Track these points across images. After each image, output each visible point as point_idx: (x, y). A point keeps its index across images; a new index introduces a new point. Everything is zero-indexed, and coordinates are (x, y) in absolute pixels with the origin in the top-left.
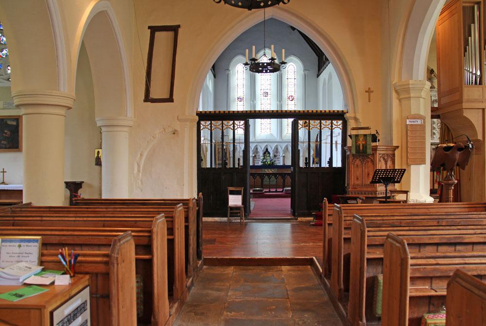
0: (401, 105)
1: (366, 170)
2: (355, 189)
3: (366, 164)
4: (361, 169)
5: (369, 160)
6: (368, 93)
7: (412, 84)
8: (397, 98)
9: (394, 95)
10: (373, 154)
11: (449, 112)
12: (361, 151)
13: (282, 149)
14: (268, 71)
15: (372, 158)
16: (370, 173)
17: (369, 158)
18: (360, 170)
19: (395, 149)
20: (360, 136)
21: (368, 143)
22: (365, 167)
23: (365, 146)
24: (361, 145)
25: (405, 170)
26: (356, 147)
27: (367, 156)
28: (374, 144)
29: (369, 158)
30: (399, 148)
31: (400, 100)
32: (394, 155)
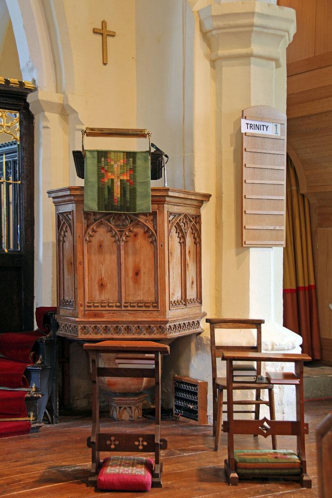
0: (217, 77)
1: (131, 259)
2: (95, 315)
3: (130, 244)
4: (115, 257)
5: (139, 230)
6: (100, 37)
7: (262, 15)
8: (207, 56)
9: (199, 47)
10: (154, 214)
11: (309, 116)
12: (117, 204)
13: (289, 41)
14: (113, 438)
15: (150, 225)
16: (143, 270)
17: (138, 224)
18: (110, 260)
19: (202, 202)
20: (112, 156)
21: (139, 179)
22: (126, 253)
23: (129, 189)
24: (117, 184)
25: (49, 193)
26: (100, 190)
27: (134, 218)
28: (154, 184)
29: (138, 224)
30: (212, 199)
31: (213, 63)
32: (197, 218)
